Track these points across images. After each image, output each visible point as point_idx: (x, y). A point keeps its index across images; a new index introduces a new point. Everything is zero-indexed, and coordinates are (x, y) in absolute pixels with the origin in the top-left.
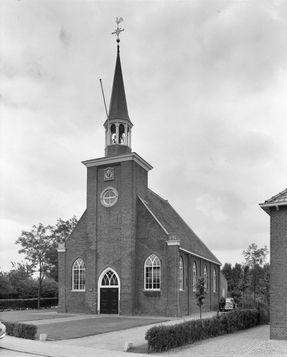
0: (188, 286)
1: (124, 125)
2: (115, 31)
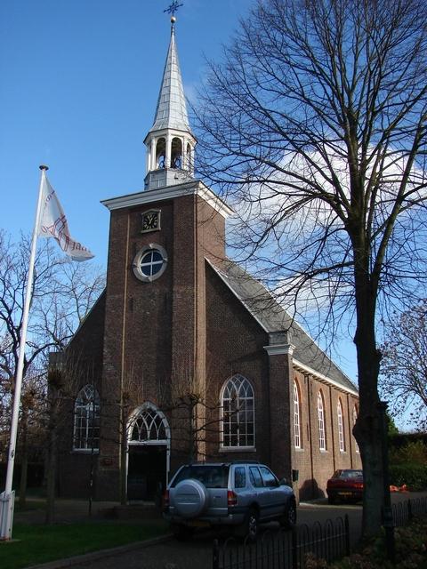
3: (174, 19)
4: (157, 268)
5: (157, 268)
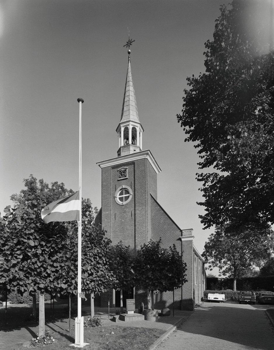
3: (130, 51)
4: (127, 198)
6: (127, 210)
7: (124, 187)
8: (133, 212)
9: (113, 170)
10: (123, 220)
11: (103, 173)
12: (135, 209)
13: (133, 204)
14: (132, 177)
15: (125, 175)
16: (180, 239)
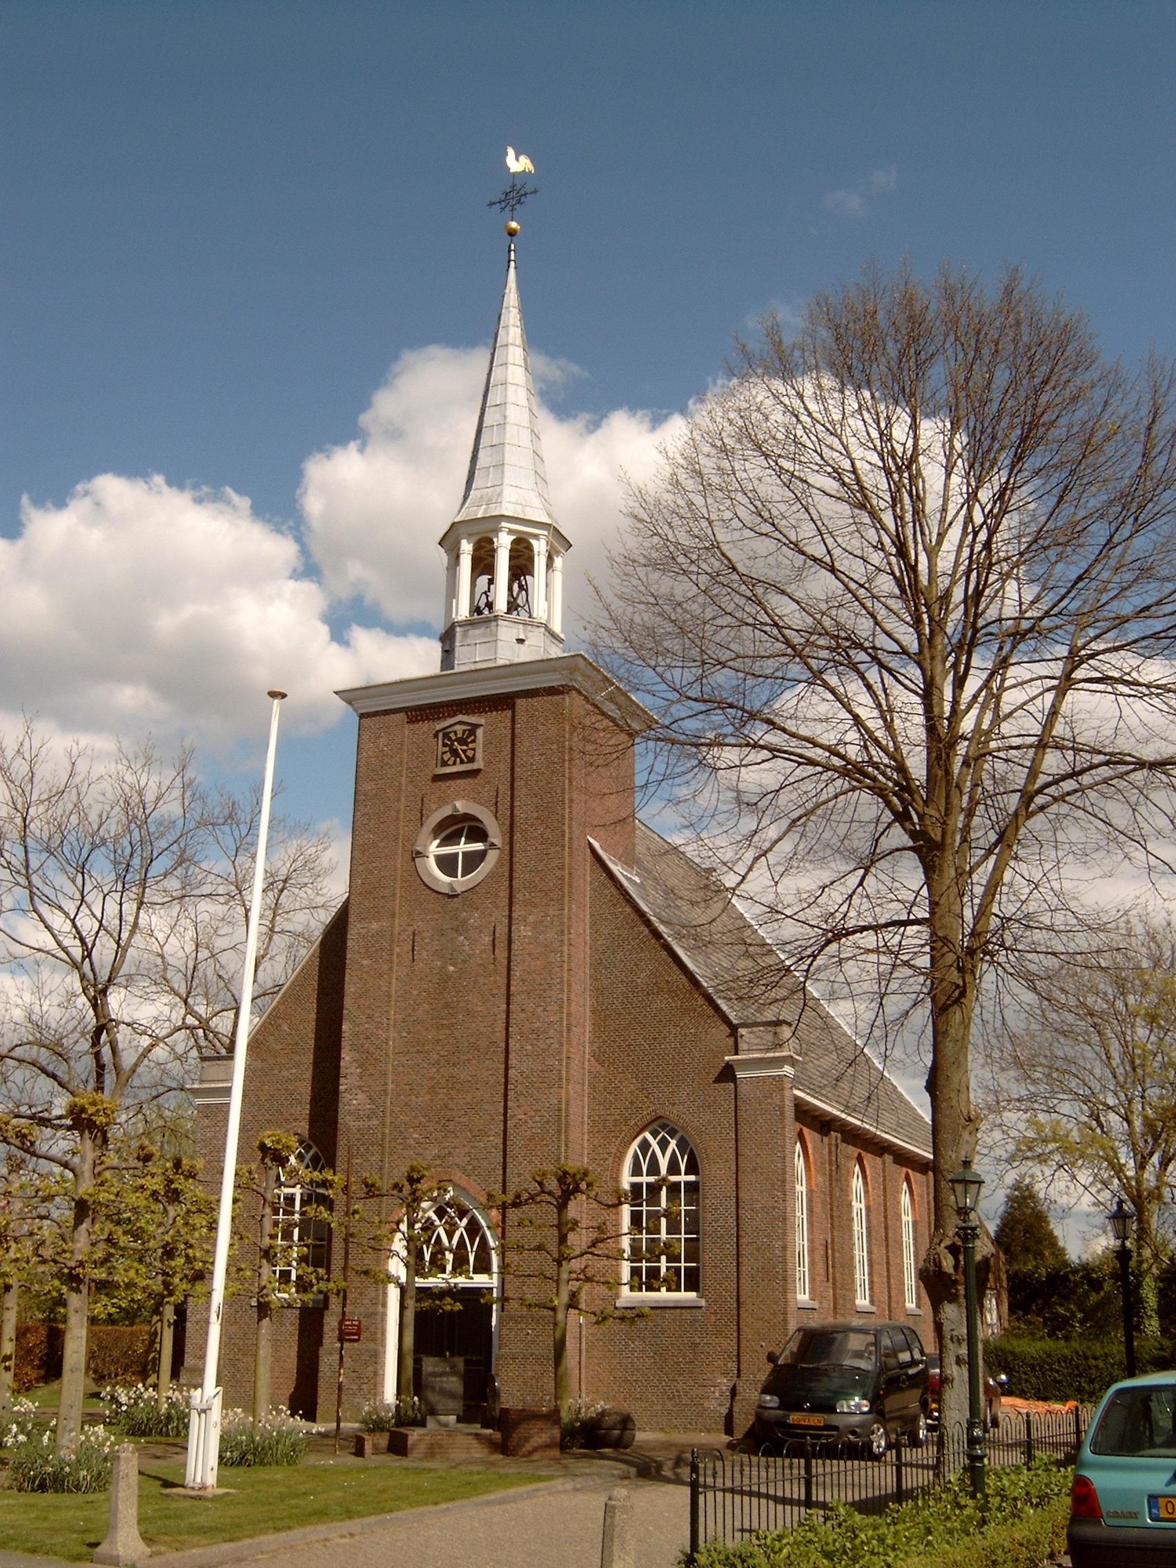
0: (834, 1278)
1: (533, 542)
2: (503, 197)
3: (514, 225)
4: (473, 860)
5: (473, 860)
6: (474, 919)
7: (461, 806)
8: (502, 931)
9: (412, 726)
10: (451, 968)
11: (365, 737)
12: (510, 917)
13: (504, 894)
14: (502, 766)
15: (470, 753)
16: (727, 1074)
